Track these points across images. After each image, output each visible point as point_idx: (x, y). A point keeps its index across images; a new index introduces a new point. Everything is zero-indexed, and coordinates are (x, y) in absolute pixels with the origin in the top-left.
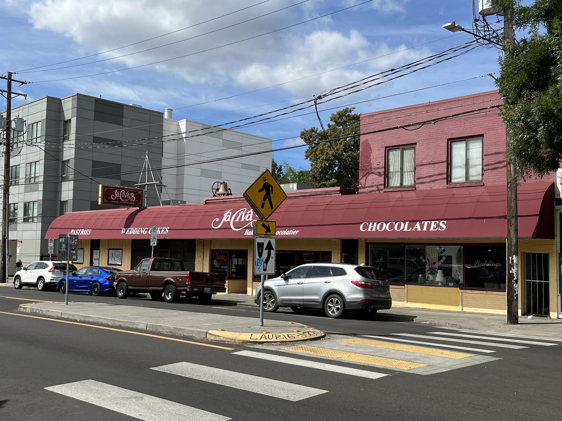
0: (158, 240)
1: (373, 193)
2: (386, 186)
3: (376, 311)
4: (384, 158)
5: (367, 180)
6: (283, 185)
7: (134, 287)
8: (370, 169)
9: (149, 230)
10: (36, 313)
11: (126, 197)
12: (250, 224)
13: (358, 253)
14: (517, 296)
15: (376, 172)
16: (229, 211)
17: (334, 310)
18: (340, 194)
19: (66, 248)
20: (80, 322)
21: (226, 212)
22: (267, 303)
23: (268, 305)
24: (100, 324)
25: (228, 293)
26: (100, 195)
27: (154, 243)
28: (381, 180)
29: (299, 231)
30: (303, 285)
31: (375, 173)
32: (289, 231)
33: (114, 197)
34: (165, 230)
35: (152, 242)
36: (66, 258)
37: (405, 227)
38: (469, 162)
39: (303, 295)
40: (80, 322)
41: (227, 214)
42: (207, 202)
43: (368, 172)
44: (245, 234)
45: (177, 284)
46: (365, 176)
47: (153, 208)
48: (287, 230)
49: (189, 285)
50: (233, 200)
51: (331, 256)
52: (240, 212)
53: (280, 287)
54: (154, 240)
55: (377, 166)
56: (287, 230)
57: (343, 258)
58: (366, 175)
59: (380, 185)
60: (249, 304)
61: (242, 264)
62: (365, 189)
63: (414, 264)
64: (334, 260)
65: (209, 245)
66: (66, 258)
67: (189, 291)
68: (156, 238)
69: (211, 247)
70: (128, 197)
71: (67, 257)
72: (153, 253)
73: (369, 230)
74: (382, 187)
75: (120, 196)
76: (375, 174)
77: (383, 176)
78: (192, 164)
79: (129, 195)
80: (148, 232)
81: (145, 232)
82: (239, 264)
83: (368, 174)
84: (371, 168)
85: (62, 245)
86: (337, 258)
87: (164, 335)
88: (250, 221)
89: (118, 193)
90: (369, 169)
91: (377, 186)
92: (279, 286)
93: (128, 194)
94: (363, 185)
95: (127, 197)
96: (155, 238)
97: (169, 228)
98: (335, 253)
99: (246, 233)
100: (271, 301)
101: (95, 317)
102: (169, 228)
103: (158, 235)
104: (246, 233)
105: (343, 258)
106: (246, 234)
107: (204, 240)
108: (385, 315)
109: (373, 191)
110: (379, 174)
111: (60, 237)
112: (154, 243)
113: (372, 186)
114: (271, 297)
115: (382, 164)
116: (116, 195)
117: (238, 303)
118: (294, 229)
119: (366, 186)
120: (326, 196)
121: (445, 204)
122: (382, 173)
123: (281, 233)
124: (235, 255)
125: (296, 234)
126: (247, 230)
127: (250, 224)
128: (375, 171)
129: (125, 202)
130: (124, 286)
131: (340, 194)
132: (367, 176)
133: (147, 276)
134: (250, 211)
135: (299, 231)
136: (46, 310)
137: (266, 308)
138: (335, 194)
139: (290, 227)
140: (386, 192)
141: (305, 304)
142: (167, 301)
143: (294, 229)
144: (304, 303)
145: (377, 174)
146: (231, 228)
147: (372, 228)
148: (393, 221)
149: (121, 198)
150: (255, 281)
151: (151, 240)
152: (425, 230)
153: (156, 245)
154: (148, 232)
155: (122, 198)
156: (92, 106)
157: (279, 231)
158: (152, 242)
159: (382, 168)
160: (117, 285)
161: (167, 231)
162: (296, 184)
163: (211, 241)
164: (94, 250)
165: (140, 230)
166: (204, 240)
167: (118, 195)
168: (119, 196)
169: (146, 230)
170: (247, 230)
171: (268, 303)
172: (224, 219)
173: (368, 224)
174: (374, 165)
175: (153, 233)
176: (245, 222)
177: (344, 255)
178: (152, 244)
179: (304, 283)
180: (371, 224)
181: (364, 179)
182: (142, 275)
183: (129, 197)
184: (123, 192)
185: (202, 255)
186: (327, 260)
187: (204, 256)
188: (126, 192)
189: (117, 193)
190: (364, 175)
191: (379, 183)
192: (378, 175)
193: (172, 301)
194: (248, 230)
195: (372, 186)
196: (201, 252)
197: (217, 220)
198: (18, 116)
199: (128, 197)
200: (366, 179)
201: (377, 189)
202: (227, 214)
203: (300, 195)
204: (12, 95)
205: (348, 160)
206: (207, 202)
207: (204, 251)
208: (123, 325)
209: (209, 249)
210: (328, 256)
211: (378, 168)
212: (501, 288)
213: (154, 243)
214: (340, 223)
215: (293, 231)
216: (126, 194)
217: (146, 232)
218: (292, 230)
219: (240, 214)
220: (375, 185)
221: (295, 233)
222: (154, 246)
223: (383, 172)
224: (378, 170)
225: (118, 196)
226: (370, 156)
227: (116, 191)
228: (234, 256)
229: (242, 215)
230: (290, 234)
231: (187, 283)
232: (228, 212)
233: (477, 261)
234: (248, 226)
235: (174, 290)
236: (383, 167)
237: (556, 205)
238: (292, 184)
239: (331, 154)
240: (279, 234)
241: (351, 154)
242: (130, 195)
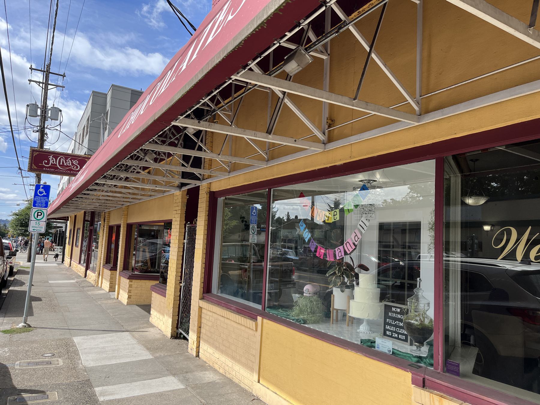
11: (65, 164)
33: (48, 163)
75: (56, 162)
79: (70, 162)
88: (70, 166)
108: (378, 359)
116: (51, 162)
129: (65, 170)
149: (58, 166)
155: (60, 165)
156: (130, 92)
167: (53, 162)
168: (55, 163)
182: (444, 294)
183: (71, 165)
184: (62, 159)
188: (66, 159)
189: (52, 159)
198: (54, 105)
204: (50, 87)
216: (66, 161)
219: (62, 161)
233: (514, 234)
237: (342, 21)
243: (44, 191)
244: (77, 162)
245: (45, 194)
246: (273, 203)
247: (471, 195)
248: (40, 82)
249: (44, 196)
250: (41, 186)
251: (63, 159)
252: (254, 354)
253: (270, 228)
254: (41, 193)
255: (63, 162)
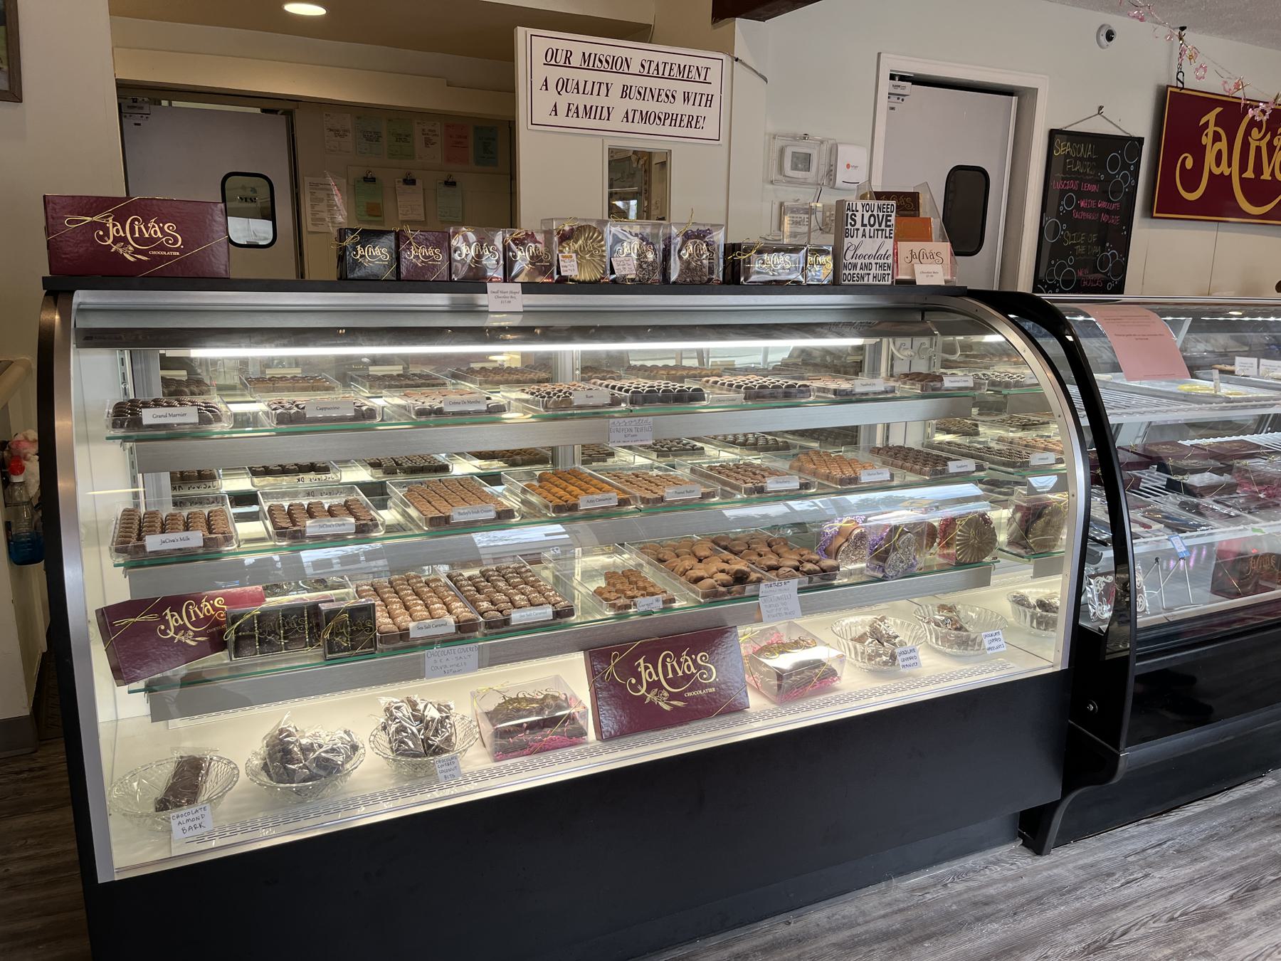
14: (1000, 440)
37: (165, 253)
38: (265, 347)
63: (950, 534)
70: (689, 670)
89: (650, 666)
93: (206, 606)
95: (684, 672)
168: (654, 677)
184: (668, 660)
189: (646, 668)
199: (689, 670)
212: (861, 362)
225: (651, 677)
227: (641, 661)
242: (694, 662)
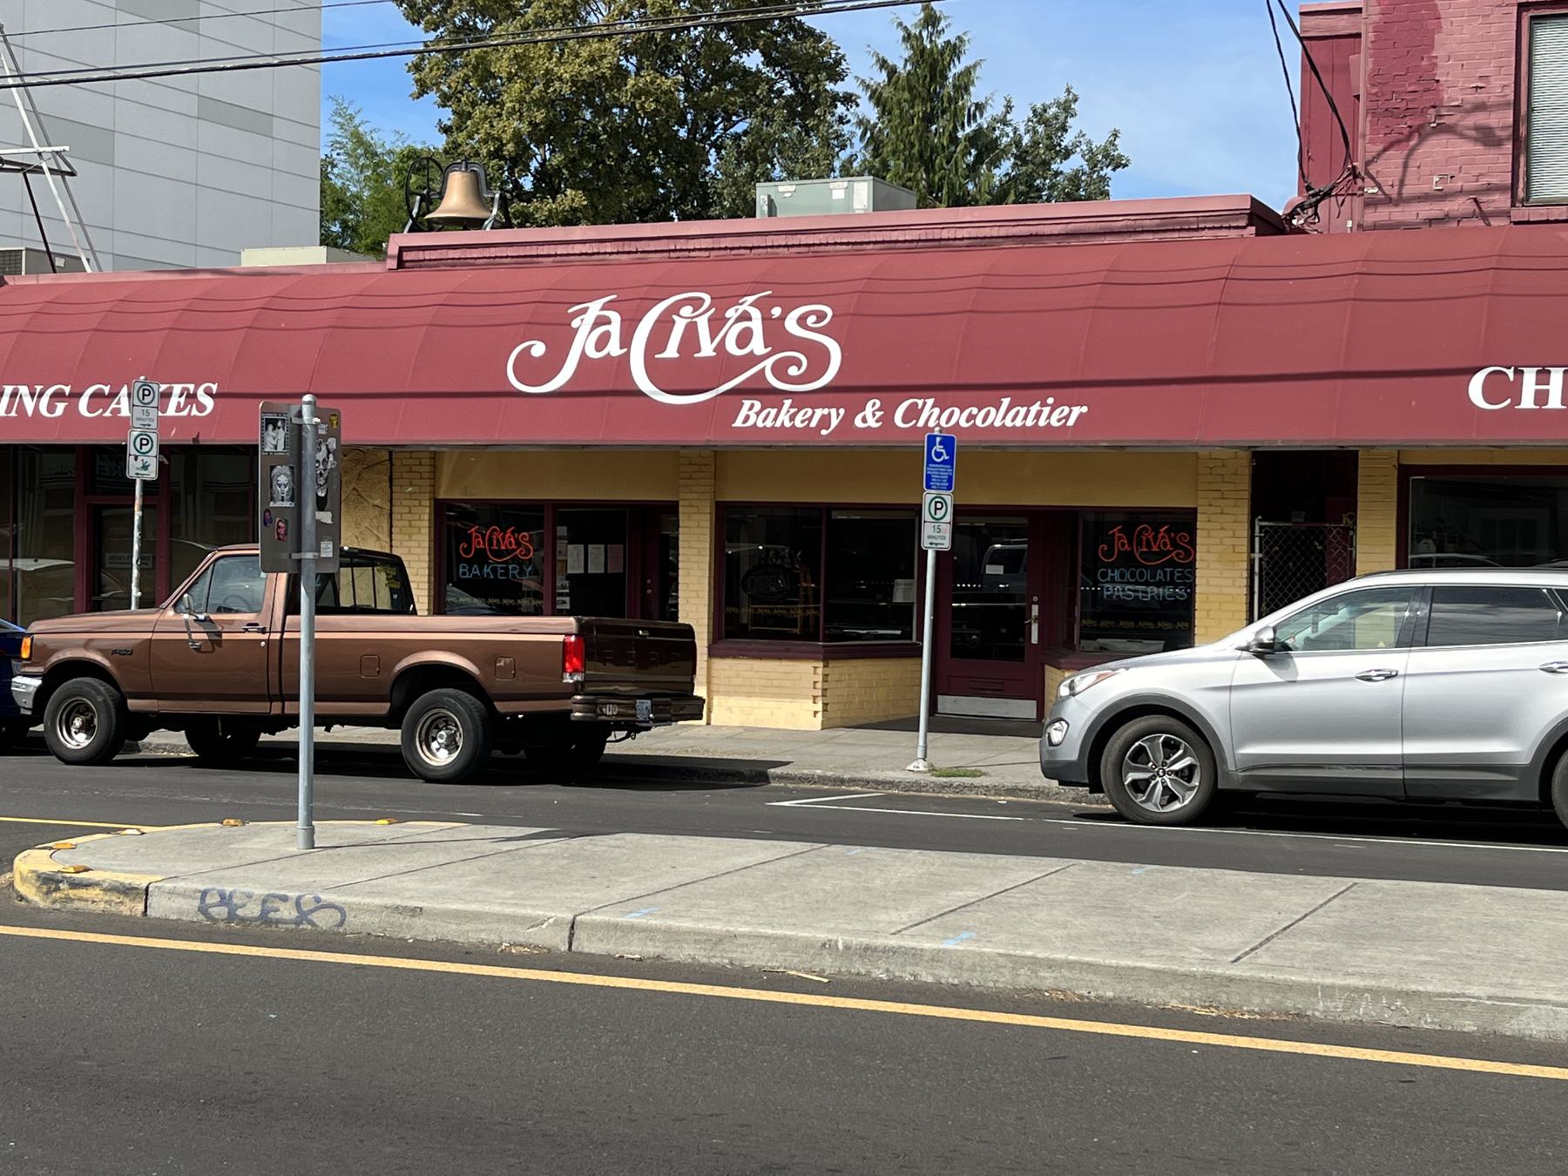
0: (164, 450)
1: (1452, 228)
2: (1521, 194)
3: (259, 737)
4: (1513, 59)
5: (1411, 163)
6: (793, 188)
7: (161, 702)
8: (1432, 110)
9: (76, 395)
10: (269, 922)
12: (763, 369)
13: (1354, 518)
15: (1469, 128)
16: (751, 299)
17: (1166, 788)
18: (1252, 229)
19: (296, 494)
20: (835, 987)
21: (584, 311)
22: (1153, 777)
23: (1160, 787)
24: (412, 946)
25: (822, 729)
26: (55, 192)
27: (145, 467)
28: (1497, 164)
29: (1085, 409)
30: (1396, 683)
31: (1459, 129)
32: (1023, 410)
34: (191, 397)
35: (136, 458)
36: (295, 556)
39: (1402, 731)
40: (835, 987)
41: (590, 318)
42: (407, 256)
43: (1421, 126)
44: (738, 423)
45: (496, 684)
46: (1398, 142)
47: (50, 282)
48: (1006, 401)
49: (578, 688)
50: (578, 249)
51: (1192, 531)
52: (675, 309)
53: (1236, 695)
54: (145, 449)
55: (1473, 98)
56: (1006, 401)
57: (1257, 540)
58: (1409, 137)
59: (1490, 189)
60: (846, 776)
61: (603, 571)
62: (1400, 209)
64: (1213, 549)
65: (427, 475)
66: (295, 556)
67: (579, 722)
68: (154, 436)
69: (434, 486)
71: (299, 551)
72: (142, 518)
73: (1527, 402)
74: (1502, 201)
76: (1462, 136)
77: (1509, 146)
78: (342, 54)
79: (756, 325)
80: (72, 411)
81: (51, 409)
82: (590, 571)
83: (1421, 133)
84: (1434, 107)
85: (275, 471)
86: (1229, 541)
87: (1246, 1029)
88: (753, 359)
90: (1423, 112)
91: (1476, 196)
92: (1230, 688)
94: (1387, 189)
95: (721, 347)
96: (150, 440)
97: (214, 388)
98: (1213, 518)
99: (747, 418)
100: (1177, 767)
101: (981, 954)
102: (214, 388)
103: (165, 423)
104: (747, 418)
105: (1257, 540)
106: (988, 423)
107: (390, 453)
109: (1446, 218)
110: (1487, 137)
111: (268, 422)
112: (145, 467)
113: (1442, 196)
114: (1141, 749)
115: (1501, 87)
117: (778, 771)
118: (1050, 401)
119: (1407, 191)
120: (1217, 239)
121: (424, 325)
122: (1499, 133)
123: (971, 417)
124: (565, 528)
125: (1071, 423)
126: (747, 403)
127: (763, 369)
128: (1463, 118)
130: (100, 699)
131: (1252, 229)
132: (1412, 143)
133: (268, 641)
134: (741, 308)
135: (1085, 409)
136: (378, 901)
137: (1149, 806)
138: (1221, 228)
139: (1025, 390)
140: (1528, 222)
141: (1417, 783)
142: (431, 774)
143: (1050, 401)
144: (1410, 775)
145: (1473, 133)
146: (641, 394)
147: (1542, 397)
148: (1508, 364)
150: (723, 656)
151: (132, 450)
152: (1559, 406)
153: (152, 474)
154: (72, 411)
157: (957, 411)
158: (136, 458)
159: (1501, 106)
160: (41, 695)
161: (209, 403)
162: (865, 184)
163: (435, 457)
164: (1035, 702)
165: (14, 395)
166: (392, 451)
168: (614, 348)
169: (58, 396)
170: (747, 403)
171: (1159, 779)
172: (583, 343)
173: (1510, 373)
174: (1455, 87)
175: (141, 416)
176: (725, 364)
177: (1261, 528)
178: (133, 469)
179: (1405, 676)
180: (1530, 375)
181: (1395, 158)
183: (757, 345)
184: (687, 311)
185: (386, 526)
186: (1155, 549)
187: (394, 530)
190: (1394, 137)
191: (1484, 181)
192: (1476, 140)
193: (462, 775)
194: (758, 406)
195: (1442, 196)
196: (374, 512)
197: (538, 349)
200: (1408, 157)
201: (1472, 207)
202: (590, 318)
203: (1003, 232)
205: (642, 107)
206: (407, 256)
207: (392, 506)
208: (1319, 1009)
209: (428, 496)
210: (513, 532)
211: (1480, 107)
213: (143, 466)
214: (1341, 368)
215: (1046, 410)
216: (717, 323)
217: (60, 407)
218: (1044, 404)
220: (1461, 192)
221: (810, 419)
222: (145, 484)
223: (1503, 128)
224: (1480, 118)
226: (1431, 47)
228: (562, 531)
229: (691, 329)
230: (1029, 423)
231: (568, 680)
232: (595, 308)
234: (743, 382)
235: (471, 716)
236: (1508, 104)
238: (846, 184)
239: (566, 76)
240: (963, 424)
241: (652, 82)
243: (943, 451)
244: (821, 316)
245: (947, 458)
246: (74, 264)
247: (20, 652)
248: (1402, 183)
249: (944, 462)
250: (938, 439)
251: (696, 303)
252: (1077, 689)
253: (1410, 557)
254: (939, 455)
255: (691, 329)
